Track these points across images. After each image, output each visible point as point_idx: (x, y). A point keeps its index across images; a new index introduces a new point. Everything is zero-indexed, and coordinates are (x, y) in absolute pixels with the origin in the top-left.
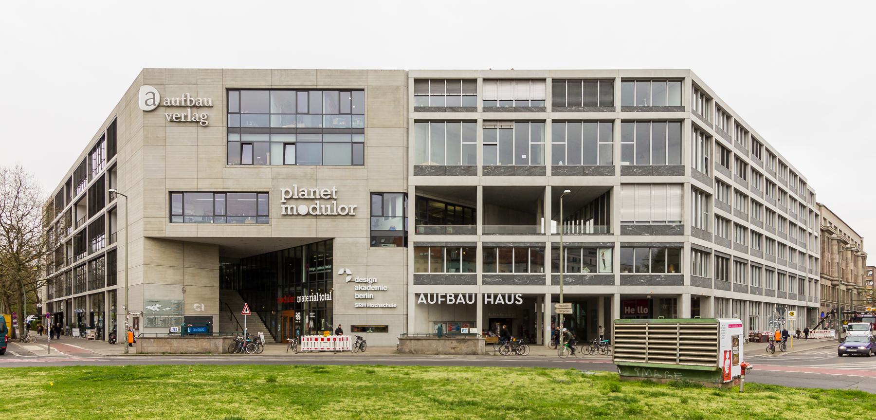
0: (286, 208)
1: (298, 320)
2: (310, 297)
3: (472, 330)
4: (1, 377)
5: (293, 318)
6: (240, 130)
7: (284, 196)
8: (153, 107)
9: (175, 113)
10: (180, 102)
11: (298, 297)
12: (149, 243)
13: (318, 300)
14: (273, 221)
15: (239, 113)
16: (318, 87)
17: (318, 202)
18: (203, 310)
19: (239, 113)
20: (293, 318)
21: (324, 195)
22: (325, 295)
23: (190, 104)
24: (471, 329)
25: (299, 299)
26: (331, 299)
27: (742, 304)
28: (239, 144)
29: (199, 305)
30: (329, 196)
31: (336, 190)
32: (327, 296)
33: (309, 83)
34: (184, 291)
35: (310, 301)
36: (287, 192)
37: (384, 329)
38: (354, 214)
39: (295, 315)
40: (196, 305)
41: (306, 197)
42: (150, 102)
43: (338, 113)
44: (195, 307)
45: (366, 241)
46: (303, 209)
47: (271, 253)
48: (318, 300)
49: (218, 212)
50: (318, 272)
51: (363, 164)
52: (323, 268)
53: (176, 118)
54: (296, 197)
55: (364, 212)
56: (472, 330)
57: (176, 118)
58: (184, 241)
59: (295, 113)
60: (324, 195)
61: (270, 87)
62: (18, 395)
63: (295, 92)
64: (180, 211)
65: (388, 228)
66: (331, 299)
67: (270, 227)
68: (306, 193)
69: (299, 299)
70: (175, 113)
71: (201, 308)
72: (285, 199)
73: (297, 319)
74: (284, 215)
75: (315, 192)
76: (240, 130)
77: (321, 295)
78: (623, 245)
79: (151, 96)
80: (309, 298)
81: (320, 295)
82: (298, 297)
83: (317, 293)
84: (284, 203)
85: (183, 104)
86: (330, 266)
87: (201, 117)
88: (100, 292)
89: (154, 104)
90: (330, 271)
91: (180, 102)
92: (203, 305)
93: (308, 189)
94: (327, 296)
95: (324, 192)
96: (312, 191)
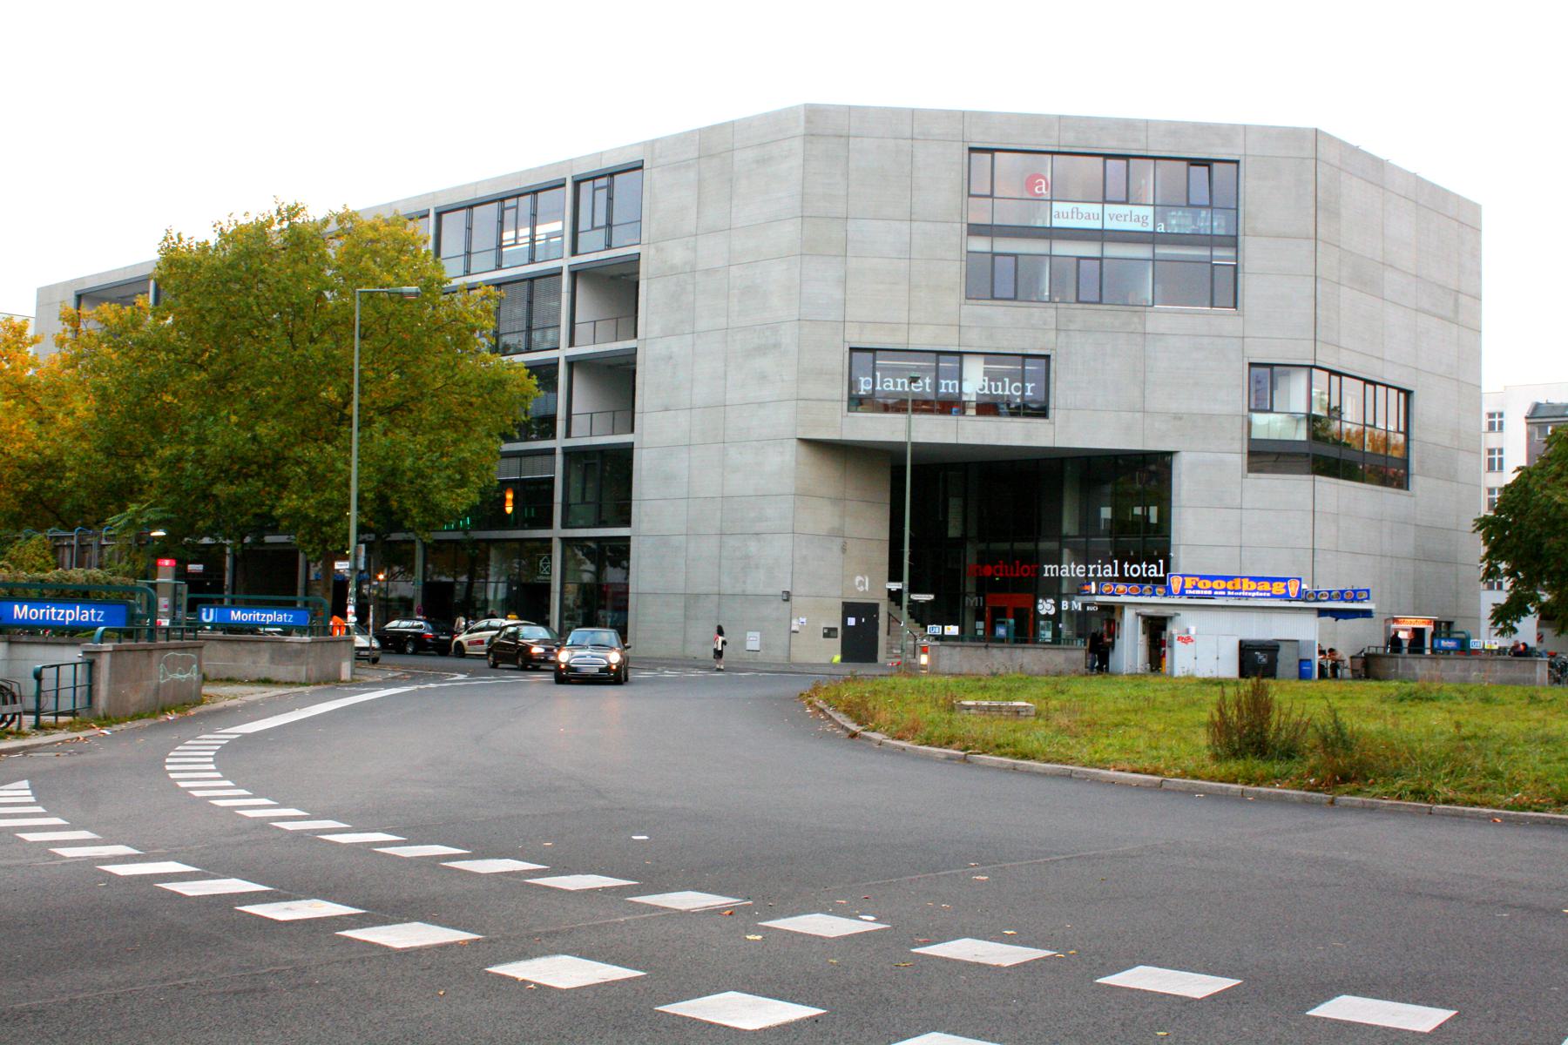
2: (1091, 567)
6: (1211, 241)
11: (1046, 567)
12: (803, 450)
15: (991, 196)
16: (1150, 154)
18: (867, 588)
19: (991, 196)
22: (1144, 566)
26: (1162, 575)
27: (590, 485)
28: (990, 256)
33: (1134, 145)
34: (844, 550)
40: (858, 578)
43: (1185, 204)
44: (857, 584)
45: (1238, 460)
49: (1367, 422)
51: (1081, 298)
59: (991, 200)
61: (1056, 149)
62: (1090, 850)
63: (1101, 159)
64: (1371, 423)
65: (1516, 453)
67: (1052, 426)
71: (864, 586)
76: (1211, 241)
81: (1126, 566)
82: (1046, 567)
88: (508, 537)
92: (867, 580)
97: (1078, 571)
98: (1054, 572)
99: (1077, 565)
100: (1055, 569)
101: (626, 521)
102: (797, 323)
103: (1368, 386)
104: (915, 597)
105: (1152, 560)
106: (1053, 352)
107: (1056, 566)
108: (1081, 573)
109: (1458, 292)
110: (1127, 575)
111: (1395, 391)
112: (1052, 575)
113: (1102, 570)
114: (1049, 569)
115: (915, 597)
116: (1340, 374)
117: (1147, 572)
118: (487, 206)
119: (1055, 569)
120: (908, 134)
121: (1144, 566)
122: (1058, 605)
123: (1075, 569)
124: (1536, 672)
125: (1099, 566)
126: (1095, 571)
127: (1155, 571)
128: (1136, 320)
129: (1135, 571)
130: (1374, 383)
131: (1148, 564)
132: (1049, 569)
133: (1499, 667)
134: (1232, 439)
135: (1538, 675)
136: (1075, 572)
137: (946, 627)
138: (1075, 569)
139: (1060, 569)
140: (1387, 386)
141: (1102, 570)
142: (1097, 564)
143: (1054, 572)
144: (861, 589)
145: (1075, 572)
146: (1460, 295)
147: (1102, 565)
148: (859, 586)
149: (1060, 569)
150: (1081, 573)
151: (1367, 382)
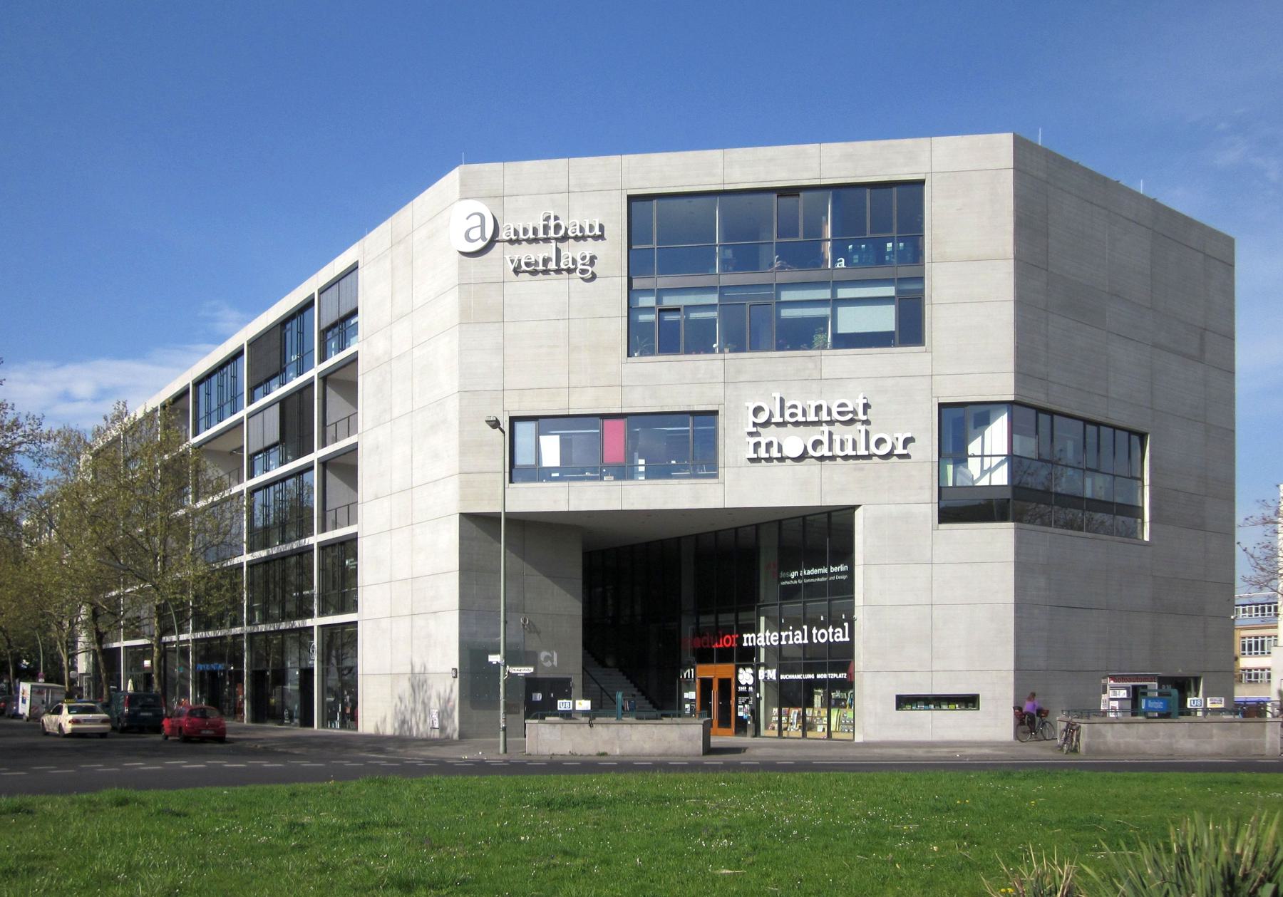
0: (757, 445)
1: (747, 685)
2: (783, 634)
3: (580, 704)
4: (3, 801)
5: (729, 680)
7: (752, 419)
8: (480, 244)
9: (526, 253)
10: (535, 231)
11: (745, 636)
13: (806, 641)
14: (726, 473)
17: (825, 428)
18: (555, 663)
20: (729, 680)
21: (840, 413)
22: (831, 630)
23: (555, 233)
24: (577, 702)
25: (748, 639)
26: (847, 639)
29: (549, 654)
30: (850, 416)
31: (865, 401)
32: (834, 633)
35: (783, 642)
36: (757, 411)
37: (970, 701)
38: (905, 452)
39: (737, 673)
41: (800, 418)
42: (475, 234)
44: (542, 659)
45: (930, 510)
46: (793, 443)
47: (662, 542)
48: (806, 641)
50: (807, 581)
52: (825, 570)
53: (527, 264)
54: (777, 419)
55: (926, 447)
56: (580, 704)
57: (527, 264)
58: (524, 521)
60: (840, 413)
66: (847, 639)
68: (799, 411)
69: (748, 639)
70: (526, 253)
71: (552, 661)
72: (755, 424)
73: (743, 682)
74: (751, 460)
75: (819, 408)
77: (771, 633)
78: (954, 501)
79: (476, 221)
80: (780, 636)
81: (814, 631)
82: (745, 636)
83: (805, 627)
84: (751, 434)
85: (541, 235)
86: (844, 568)
87: (578, 259)
89: (483, 237)
90: (844, 577)
91: (535, 231)
92: (555, 654)
93: (804, 400)
94: (834, 633)
95: (840, 406)
96: (814, 404)
97: (772, 638)
98: (752, 642)
99: (771, 633)
100: (752, 638)
101: (354, 607)
102: (458, 394)
103: (1042, 417)
104: (514, 670)
105: (838, 624)
106: (722, 407)
107: (753, 635)
108: (775, 641)
109: (1205, 329)
110: (815, 641)
111: (1126, 434)
112: (750, 644)
113: (794, 636)
114: (748, 638)
115: (514, 670)
116: (1051, 413)
117: (833, 637)
118: (678, 415)
119: (752, 638)
120: (564, 188)
121: (831, 630)
122: (755, 675)
123: (770, 637)
124: (1265, 736)
125: (790, 633)
126: (787, 637)
127: (841, 635)
128: (811, 365)
129: (823, 636)
130: (1098, 424)
131: (834, 628)
132: (748, 638)
133: (1215, 731)
134: (921, 488)
135: (1268, 739)
136: (770, 641)
137: (577, 702)
138: (770, 637)
139: (757, 638)
140: (1115, 428)
141: (794, 636)
142: (789, 630)
143: (752, 642)
144: (548, 664)
145: (770, 641)
146: (1207, 332)
147: (793, 632)
148: (546, 661)
149: (757, 638)
150: (775, 641)
151: (1087, 422)
